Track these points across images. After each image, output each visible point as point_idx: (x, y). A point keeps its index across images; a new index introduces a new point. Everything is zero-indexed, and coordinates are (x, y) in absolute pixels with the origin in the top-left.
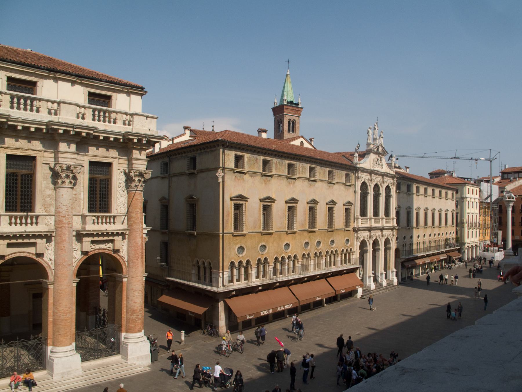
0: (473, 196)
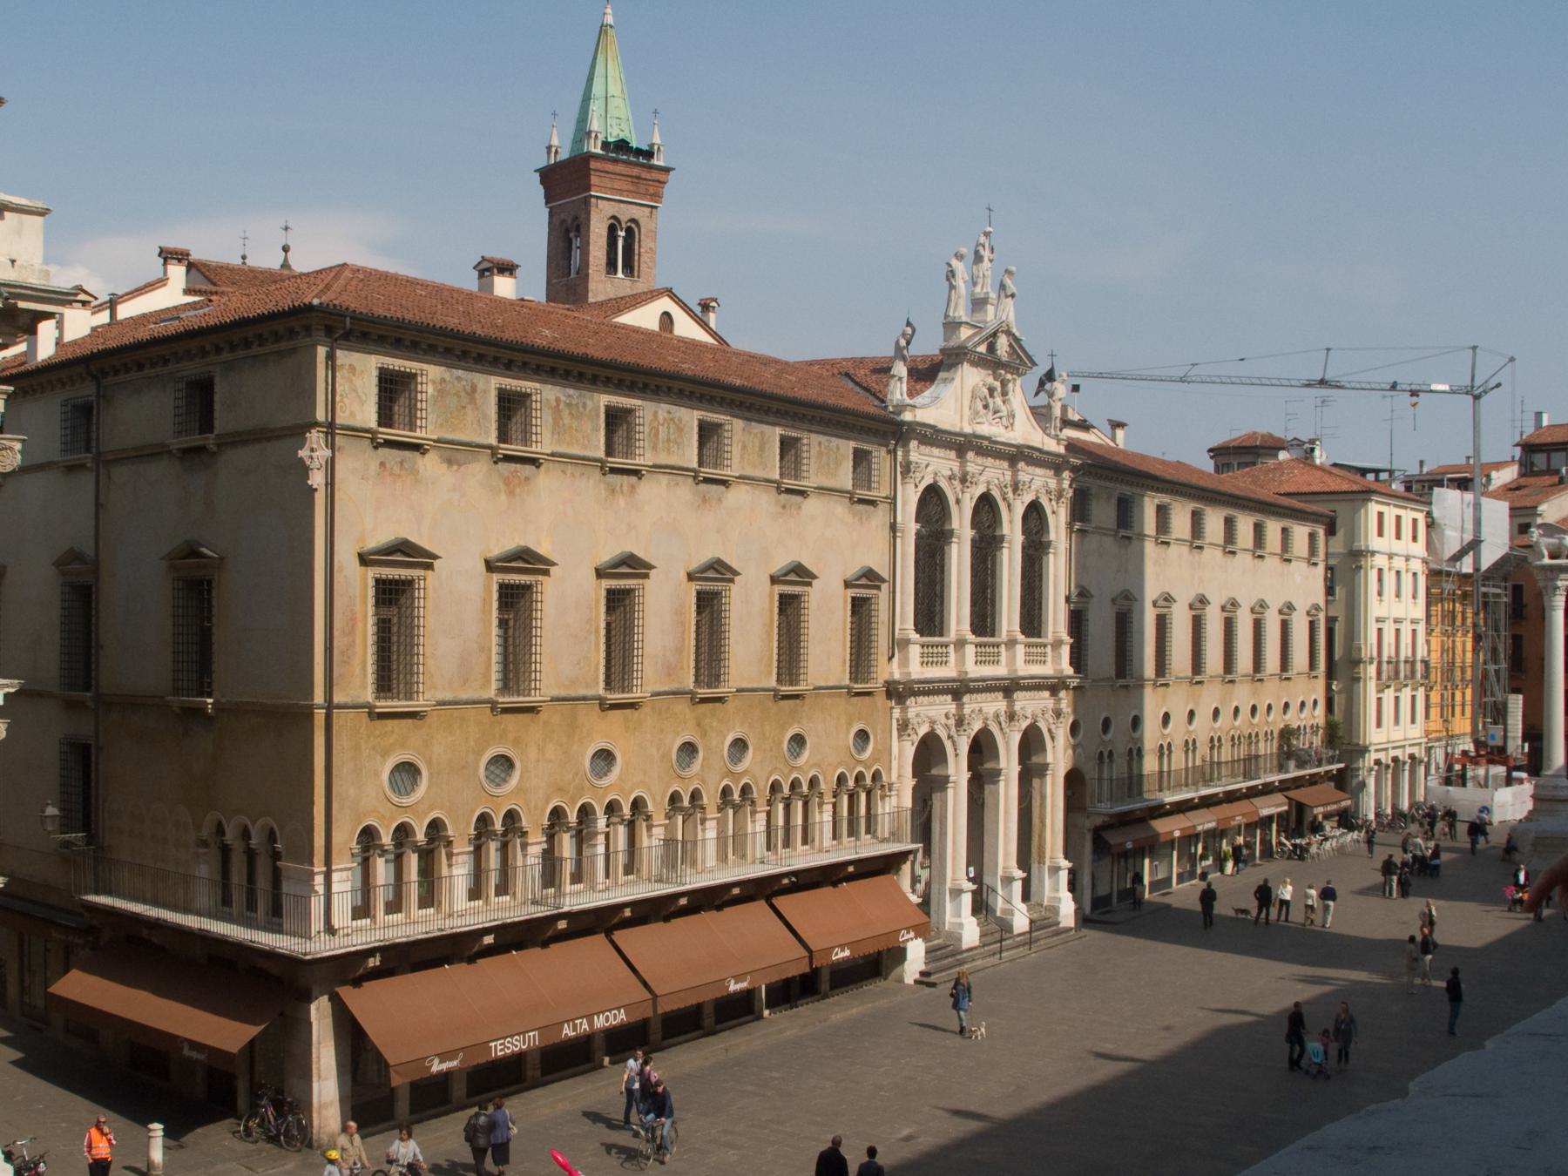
0: (1397, 547)
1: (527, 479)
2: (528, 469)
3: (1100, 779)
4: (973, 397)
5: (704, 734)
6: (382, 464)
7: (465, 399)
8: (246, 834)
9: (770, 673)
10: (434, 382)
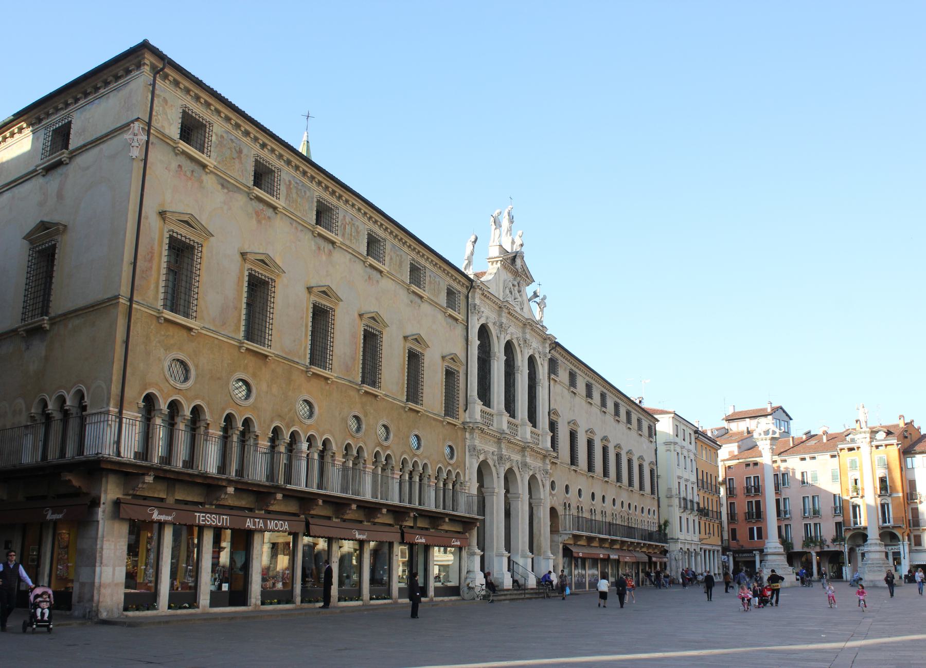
1: (269, 218)
3: (565, 515)
4: (505, 288)
5: (366, 415)
7: (235, 155)
8: (62, 400)
9: (403, 393)
10: (216, 135)
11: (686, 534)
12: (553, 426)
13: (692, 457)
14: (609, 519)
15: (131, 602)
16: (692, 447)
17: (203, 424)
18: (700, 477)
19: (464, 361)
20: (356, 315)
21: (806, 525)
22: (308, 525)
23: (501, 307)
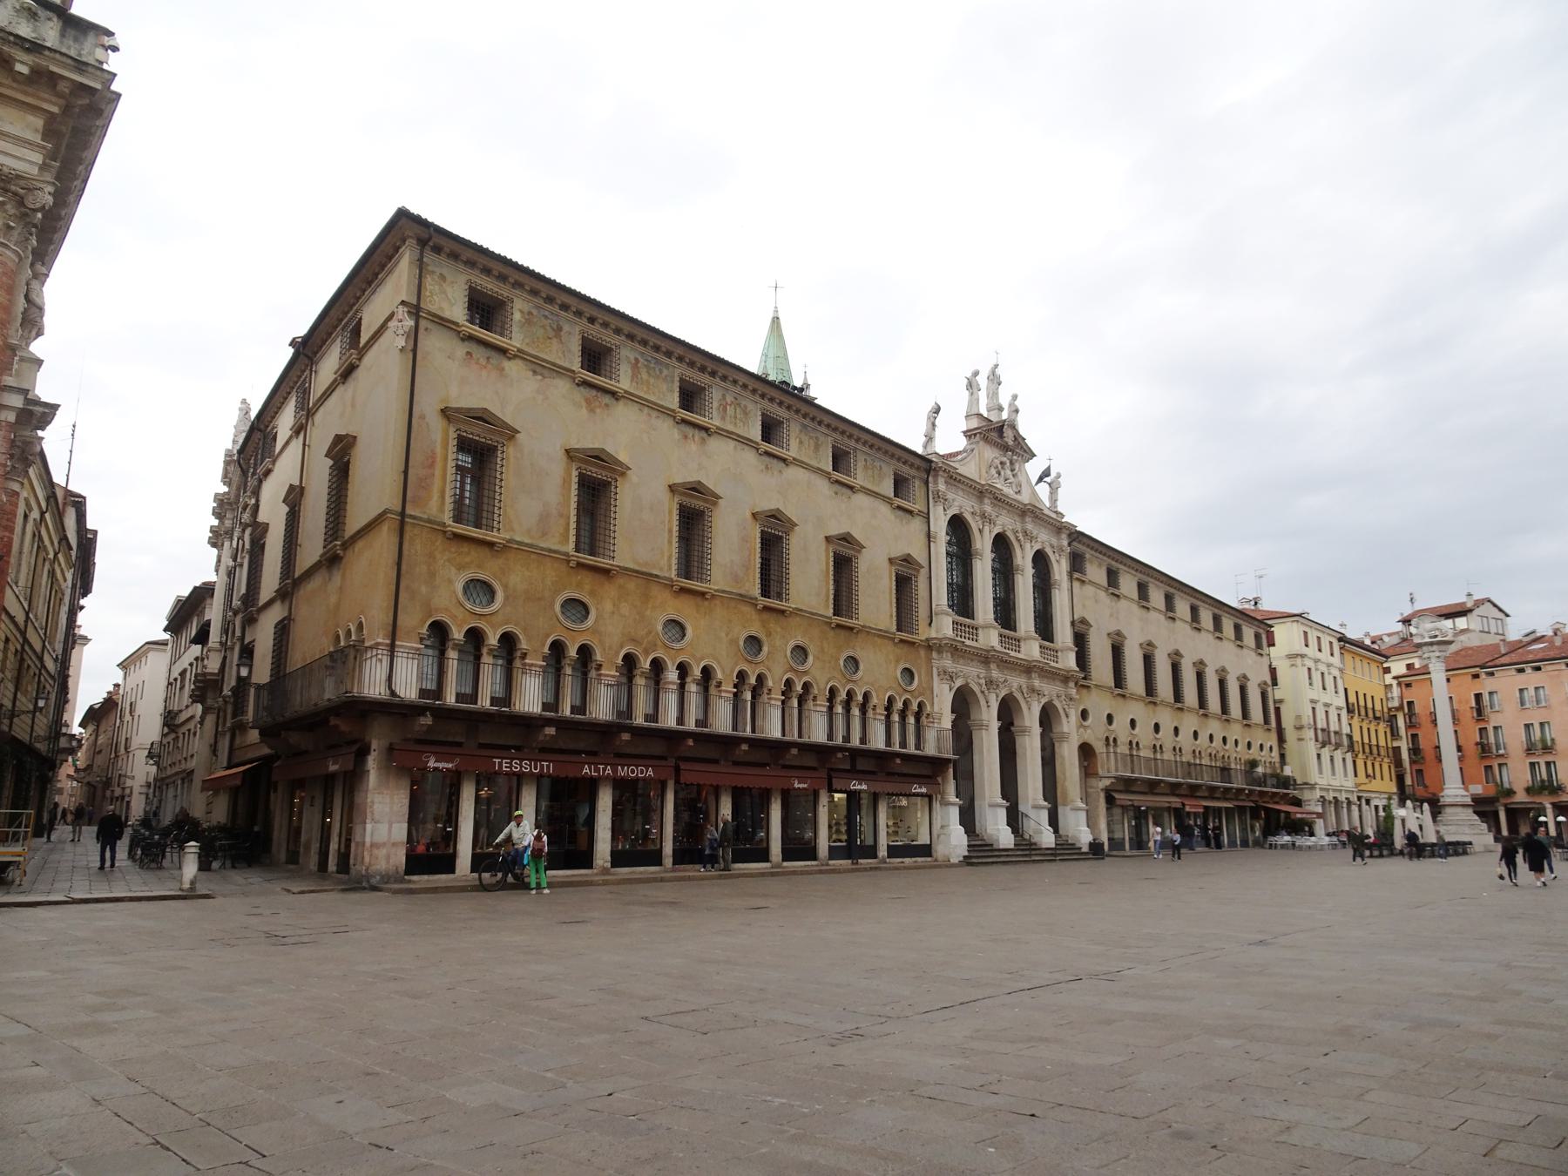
2: (607, 399)
5: (769, 634)
6: (468, 353)
7: (551, 334)
11: (1325, 775)
12: (1080, 640)
13: (1336, 673)
14: (1187, 757)
15: (417, 863)
16: (1336, 660)
17: (518, 654)
18: (1352, 699)
19: (924, 563)
20: (748, 515)
21: (1532, 765)
22: (677, 770)
23: (981, 492)
